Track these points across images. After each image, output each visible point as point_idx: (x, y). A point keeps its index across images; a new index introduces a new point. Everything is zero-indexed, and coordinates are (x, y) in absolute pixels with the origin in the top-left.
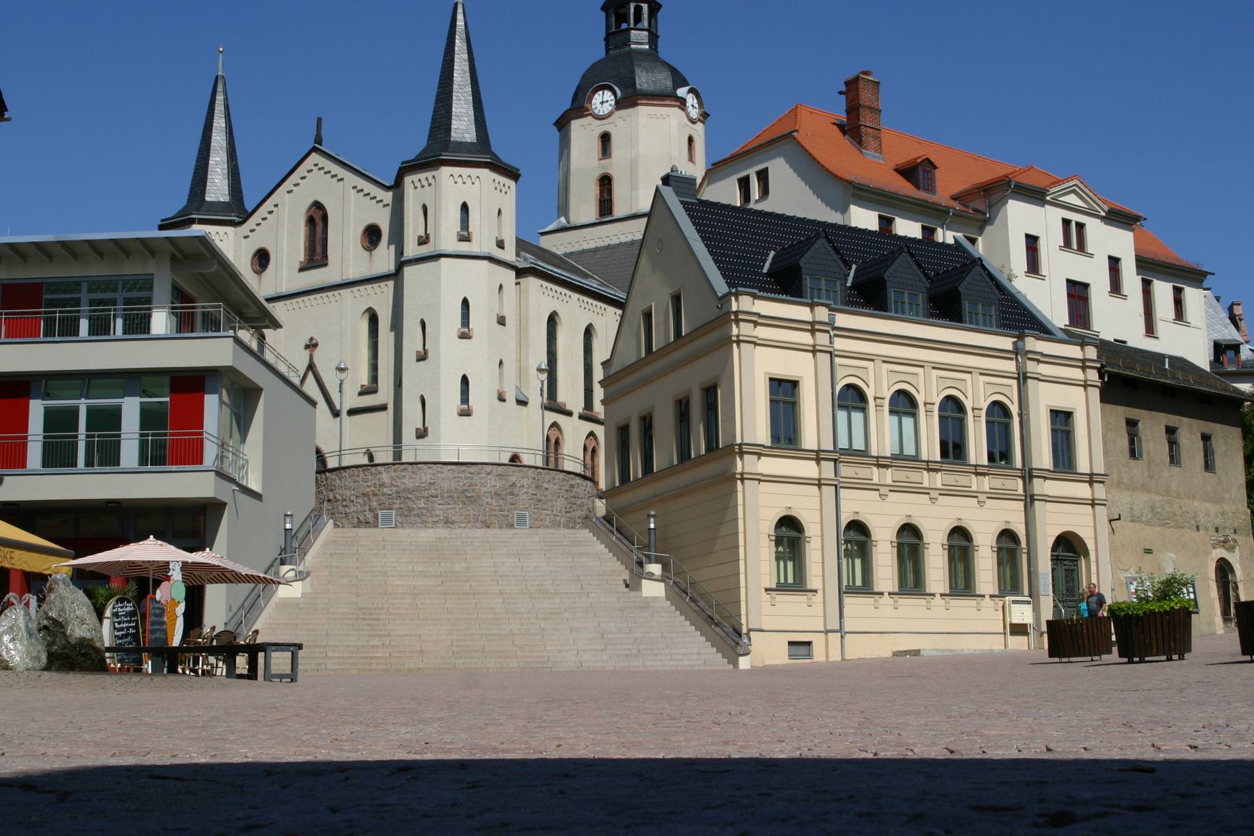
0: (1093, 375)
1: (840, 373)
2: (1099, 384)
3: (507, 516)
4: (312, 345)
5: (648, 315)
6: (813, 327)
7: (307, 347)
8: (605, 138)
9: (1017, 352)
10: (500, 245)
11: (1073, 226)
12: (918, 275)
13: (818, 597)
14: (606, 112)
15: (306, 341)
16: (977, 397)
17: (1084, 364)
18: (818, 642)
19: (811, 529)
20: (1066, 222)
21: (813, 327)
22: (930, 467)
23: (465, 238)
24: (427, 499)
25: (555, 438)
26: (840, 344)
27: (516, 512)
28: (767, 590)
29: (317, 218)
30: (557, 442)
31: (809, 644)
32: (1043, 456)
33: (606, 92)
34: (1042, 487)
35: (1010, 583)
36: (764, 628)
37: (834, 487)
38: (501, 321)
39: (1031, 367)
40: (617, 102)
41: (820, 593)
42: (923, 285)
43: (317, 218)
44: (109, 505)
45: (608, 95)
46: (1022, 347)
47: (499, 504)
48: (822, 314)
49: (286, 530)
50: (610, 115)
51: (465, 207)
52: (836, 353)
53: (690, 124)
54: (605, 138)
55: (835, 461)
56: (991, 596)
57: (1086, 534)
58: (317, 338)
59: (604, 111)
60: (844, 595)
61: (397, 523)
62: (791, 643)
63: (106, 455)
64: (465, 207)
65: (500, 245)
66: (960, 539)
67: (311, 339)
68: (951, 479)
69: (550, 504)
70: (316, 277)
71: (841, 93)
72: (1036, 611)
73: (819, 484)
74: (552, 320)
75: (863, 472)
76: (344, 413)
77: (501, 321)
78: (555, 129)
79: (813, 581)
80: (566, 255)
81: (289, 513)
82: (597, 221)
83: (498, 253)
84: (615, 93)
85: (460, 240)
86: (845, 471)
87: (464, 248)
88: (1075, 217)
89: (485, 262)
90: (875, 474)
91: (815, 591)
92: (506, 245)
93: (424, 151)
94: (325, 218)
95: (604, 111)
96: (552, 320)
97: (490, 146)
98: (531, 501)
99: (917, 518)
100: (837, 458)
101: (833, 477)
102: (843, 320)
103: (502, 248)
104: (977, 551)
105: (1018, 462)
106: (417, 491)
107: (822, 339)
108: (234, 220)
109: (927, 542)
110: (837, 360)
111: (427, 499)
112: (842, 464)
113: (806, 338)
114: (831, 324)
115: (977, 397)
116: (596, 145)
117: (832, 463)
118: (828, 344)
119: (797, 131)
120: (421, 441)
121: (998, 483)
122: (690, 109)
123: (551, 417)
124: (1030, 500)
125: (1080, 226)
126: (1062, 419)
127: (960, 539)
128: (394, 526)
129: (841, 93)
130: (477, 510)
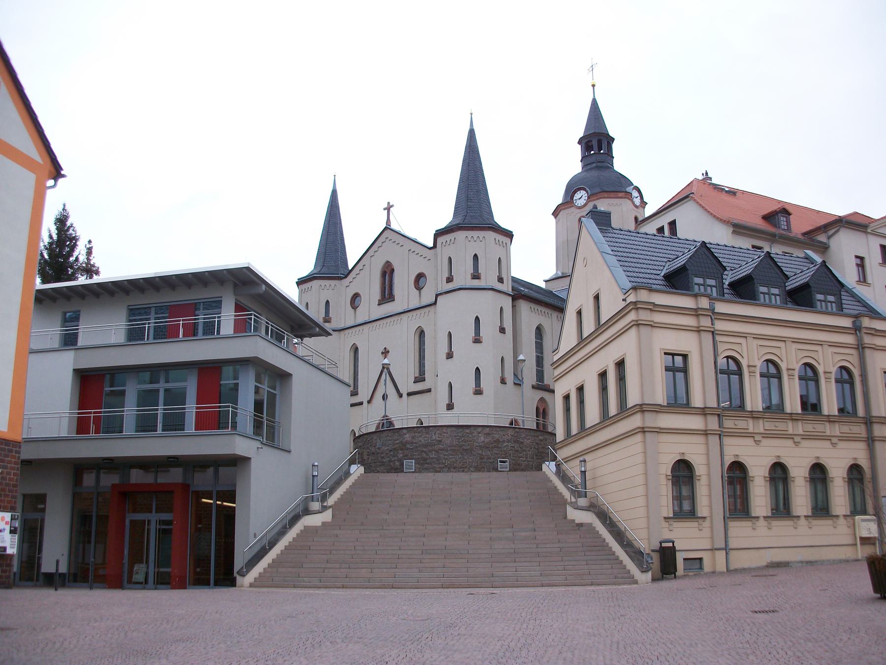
1: (721, 347)
3: (493, 462)
4: (388, 208)
5: (579, 313)
6: (696, 313)
10: (501, 280)
12: (777, 274)
13: (707, 523)
15: (382, 350)
18: (706, 557)
19: (700, 470)
21: (696, 313)
22: (793, 417)
23: (476, 276)
24: (437, 451)
25: (543, 408)
26: (720, 325)
27: (499, 460)
28: (665, 518)
29: (388, 272)
30: (544, 410)
31: (700, 559)
33: (582, 191)
37: (718, 436)
38: (502, 330)
39: (867, 340)
40: (589, 198)
41: (708, 520)
42: (781, 281)
43: (388, 272)
44: (169, 460)
45: (583, 192)
46: (860, 324)
47: (487, 454)
48: (704, 303)
49: (313, 476)
51: (476, 256)
52: (717, 332)
55: (719, 415)
56: (845, 516)
58: (388, 348)
59: (581, 204)
60: (729, 520)
61: (416, 468)
63: (174, 424)
64: (476, 256)
66: (818, 472)
67: (385, 348)
68: (809, 427)
69: (524, 453)
70: (389, 308)
73: (706, 433)
75: (741, 424)
76: (405, 395)
77: (502, 330)
78: (553, 217)
79: (702, 510)
81: (316, 464)
83: (499, 286)
84: (587, 192)
85: (473, 279)
86: (728, 423)
87: (476, 283)
89: (491, 292)
91: (705, 518)
92: (505, 281)
95: (581, 204)
96: (539, 331)
98: (511, 451)
99: (744, 457)
100: (719, 413)
101: (717, 428)
102: (721, 307)
103: (502, 282)
104: (832, 481)
105: (861, 412)
106: (429, 446)
107: (705, 322)
108: (340, 277)
109: (793, 476)
110: (718, 338)
111: (437, 451)
112: (724, 418)
113: (690, 321)
114: (712, 310)
117: (716, 418)
118: (710, 325)
119: (693, 193)
120: (450, 412)
121: (845, 429)
122: (635, 200)
123: (540, 394)
127: (818, 472)
128: (414, 470)
130: (471, 459)
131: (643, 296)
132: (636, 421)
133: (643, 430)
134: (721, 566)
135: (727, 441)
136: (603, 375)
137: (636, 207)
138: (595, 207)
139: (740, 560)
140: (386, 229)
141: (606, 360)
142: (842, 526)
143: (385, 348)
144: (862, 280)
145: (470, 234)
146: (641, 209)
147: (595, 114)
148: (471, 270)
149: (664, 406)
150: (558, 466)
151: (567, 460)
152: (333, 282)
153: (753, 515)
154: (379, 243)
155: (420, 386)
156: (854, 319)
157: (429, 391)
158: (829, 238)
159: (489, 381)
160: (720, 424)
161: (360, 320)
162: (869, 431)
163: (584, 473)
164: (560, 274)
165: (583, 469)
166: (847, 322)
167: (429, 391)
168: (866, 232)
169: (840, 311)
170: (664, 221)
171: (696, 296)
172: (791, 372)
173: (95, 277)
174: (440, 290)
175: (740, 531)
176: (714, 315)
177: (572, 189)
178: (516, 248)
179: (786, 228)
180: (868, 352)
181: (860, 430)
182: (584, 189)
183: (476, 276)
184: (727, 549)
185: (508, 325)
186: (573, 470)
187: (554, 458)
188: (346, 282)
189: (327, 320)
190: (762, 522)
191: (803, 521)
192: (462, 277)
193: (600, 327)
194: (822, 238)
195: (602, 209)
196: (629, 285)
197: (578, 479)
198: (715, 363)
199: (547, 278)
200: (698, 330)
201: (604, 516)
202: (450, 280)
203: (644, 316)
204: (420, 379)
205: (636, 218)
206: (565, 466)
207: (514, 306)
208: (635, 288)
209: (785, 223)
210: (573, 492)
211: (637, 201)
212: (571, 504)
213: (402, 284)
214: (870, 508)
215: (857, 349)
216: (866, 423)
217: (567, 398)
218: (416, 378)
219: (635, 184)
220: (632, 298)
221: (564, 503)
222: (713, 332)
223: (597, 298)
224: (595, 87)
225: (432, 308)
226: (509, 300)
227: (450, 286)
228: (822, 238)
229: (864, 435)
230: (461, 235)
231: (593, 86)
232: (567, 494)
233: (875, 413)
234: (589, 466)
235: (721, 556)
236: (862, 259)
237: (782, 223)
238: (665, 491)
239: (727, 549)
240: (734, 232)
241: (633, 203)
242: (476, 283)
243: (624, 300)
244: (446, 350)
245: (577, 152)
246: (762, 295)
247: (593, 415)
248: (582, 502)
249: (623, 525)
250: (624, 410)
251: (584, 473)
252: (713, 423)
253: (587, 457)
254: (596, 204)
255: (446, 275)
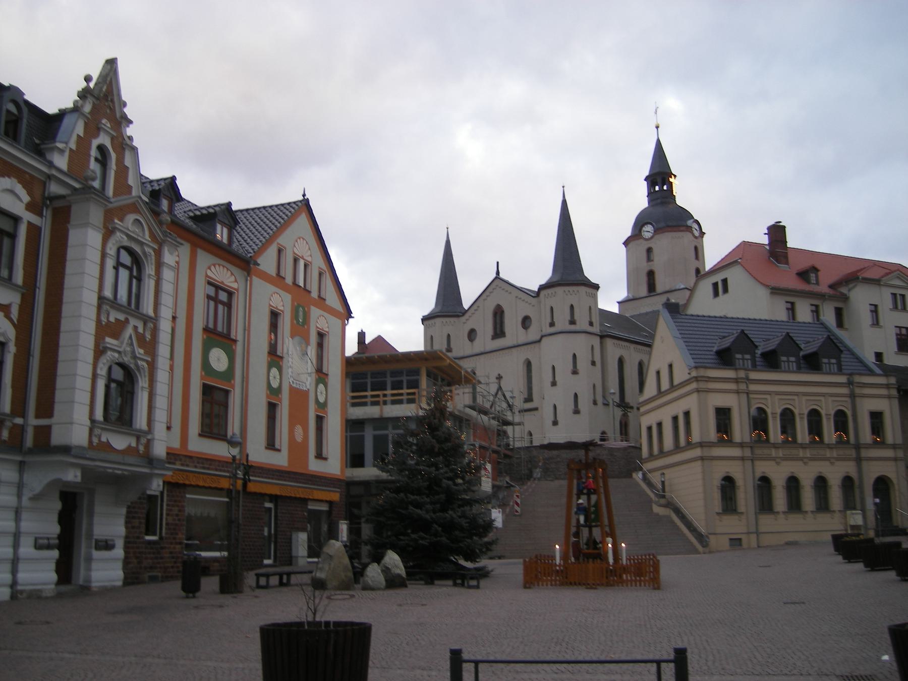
0: (894, 392)
1: (753, 402)
2: (897, 396)
5: (658, 373)
6: (736, 381)
7: (497, 378)
8: (649, 251)
9: (850, 383)
10: (591, 324)
11: (898, 296)
14: (650, 237)
16: (828, 410)
17: (888, 386)
19: (740, 482)
20: (894, 295)
21: (736, 381)
23: (573, 322)
26: (753, 387)
28: (717, 513)
29: (499, 313)
31: (740, 539)
32: (866, 435)
34: (864, 453)
35: (849, 504)
36: (717, 532)
38: (593, 363)
39: (858, 391)
40: (655, 231)
43: (499, 313)
48: (742, 374)
50: (652, 237)
53: (695, 239)
54: (649, 251)
55: (751, 447)
56: (812, 512)
57: (892, 475)
58: (502, 374)
62: (731, 539)
65: (591, 324)
66: (821, 483)
70: (500, 343)
71: (765, 234)
72: (865, 517)
73: (742, 459)
74: (621, 362)
75: (766, 451)
77: (593, 363)
79: (741, 507)
80: (632, 317)
82: (648, 295)
83: (590, 329)
84: (653, 226)
86: (758, 451)
87: (572, 328)
88: (898, 292)
89: (583, 335)
90: (773, 452)
92: (594, 324)
93: (550, 278)
94: (503, 312)
96: (621, 362)
97: (583, 272)
102: (753, 375)
107: (743, 387)
110: (751, 396)
113: (732, 386)
114: (747, 378)
115: (828, 410)
116: (644, 255)
118: (745, 388)
124: (859, 460)
125: (903, 296)
126: (876, 418)
129: (765, 234)
131: (702, 372)
132: (697, 452)
133: (702, 458)
134: (754, 544)
135: (757, 463)
136: (675, 419)
137: (696, 237)
138: (668, 300)
139: (766, 540)
140: (496, 278)
141: (678, 408)
142: (837, 516)
143: (499, 375)
144: (875, 323)
145: (567, 288)
146: (700, 239)
147: (659, 154)
148: (568, 318)
149: (715, 443)
150: (644, 475)
151: (651, 471)
152: (452, 320)
153: (775, 511)
154: (490, 289)
155: (528, 405)
156: (848, 377)
157: (536, 409)
158: (849, 290)
159: (585, 403)
160: (752, 453)
161: (477, 350)
162: (858, 453)
163: (663, 483)
164: (631, 297)
165: (663, 479)
166: (843, 379)
167: (536, 409)
168: (879, 285)
169: (840, 371)
170: (718, 278)
171: (736, 369)
172: (802, 416)
173: (114, 242)
174: (544, 332)
175: (766, 522)
176: (748, 380)
177: (640, 222)
178: (600, 294)
179: (815, 282)
180: (858, 400)
181: (853, 453)
182: (651, 224)
183: (573, 322)
184: (758, 533)
185: (598, 359)
186: (656, 478)
187: (641, 469)
188: (463, 319)
189: (449, 350)
190: (782, 516)
191: (810, 515)
192: (562, 322)
193: (673, 387)
194: (844, 290)
195: (673, 301)
196: (693, 365)
197: (660, 486)
198: (749, 413)
199: (620, 300)
200: (738, 392)
201: (678, 511)
202: (552, 324)
203: (703, 385)
204: (529, 399)
205: (698, 271)
206: (649, 475)
207: (601, 343)
208: (696, 368)
209: (814, 279)
210: (656, 495)
211: (697, 234)
212: (656, 503)
213: (512, 324)
214: (858, 505)
215: (850, 397)
216: (855, 448)
217: (650, 429)
218: (525, 398)
219: (695, 218)
220: (694, 374)
221: (650, 501)
222: (747, 393)
223: (671, 366)
224: (659, 129)
225: (537, 345)
226: (598, 339)
227: (552, 330)
228: (844, 290)
229: (854, 455)
230: (560, 290)
231: (657, 127)
232: (652, 495)
233: (862, 441)
234: (667, 476)
235: (753, 537)
236: (876, 306)
237: (812, 278)
238: (717, 495)
239: (758, 533)
240: (772, 293)
241: (693, 235)
242: (572, 328)
243: (689, 374)
244: (551, 379)
245: (644, 187)
246: (783, 363)
247: (668, 442)
248: (662, 501)
249: (690, 517)
250: (690, 445)
251: (663, 483)
252: (748, 453)
253: (665, 471)
254: (670, 298)
255: (549, 320)
